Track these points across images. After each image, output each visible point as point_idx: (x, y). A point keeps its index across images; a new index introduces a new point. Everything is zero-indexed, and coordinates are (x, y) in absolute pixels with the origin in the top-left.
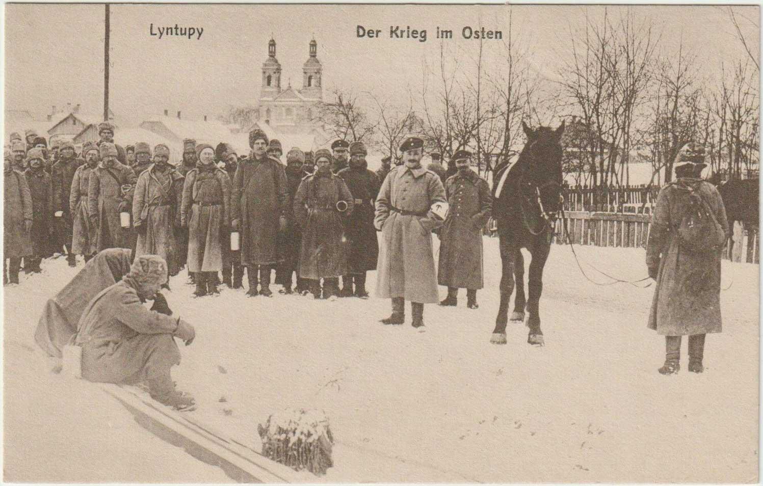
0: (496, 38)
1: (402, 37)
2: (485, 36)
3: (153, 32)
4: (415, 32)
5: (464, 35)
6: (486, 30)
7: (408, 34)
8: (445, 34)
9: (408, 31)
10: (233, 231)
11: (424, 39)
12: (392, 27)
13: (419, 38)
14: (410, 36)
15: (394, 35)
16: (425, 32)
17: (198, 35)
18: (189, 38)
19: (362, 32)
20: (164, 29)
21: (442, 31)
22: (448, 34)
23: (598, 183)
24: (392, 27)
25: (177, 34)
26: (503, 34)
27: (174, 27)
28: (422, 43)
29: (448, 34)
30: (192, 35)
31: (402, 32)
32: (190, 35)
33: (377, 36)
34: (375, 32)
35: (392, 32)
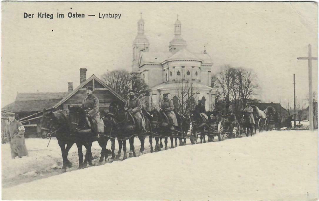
0: (82, 17)
1: (43, 17)
2: (78, 16)
3: (100, 17)
4: (80, 15)
5: (69, 17)
6: (78, 14)
7: (45, 16)
8: (60, 16)
9: (45, 15)
10: (292, 120)
11: (52, 18)
12: (39, 13)
13: (50, 18)
14: (46, 16)
15: (39, 16)
16: (52, 15)
17: (119, 17)
18: (115, 18)
19: (26, 15)
20: (104, 14)
21: (113, 17)
22: (62, 15)
23: (128, 142)
24: (39, 13)
25: (77, 17)
26: (64, 16)
27: (75, 14)
28: (51, 20)
29: (62, 15)
30: (116, 17)
31: (43, 15)
32: (115, 17)
33: (32, 17)
34: (81, 15)
35: (39, 15)
